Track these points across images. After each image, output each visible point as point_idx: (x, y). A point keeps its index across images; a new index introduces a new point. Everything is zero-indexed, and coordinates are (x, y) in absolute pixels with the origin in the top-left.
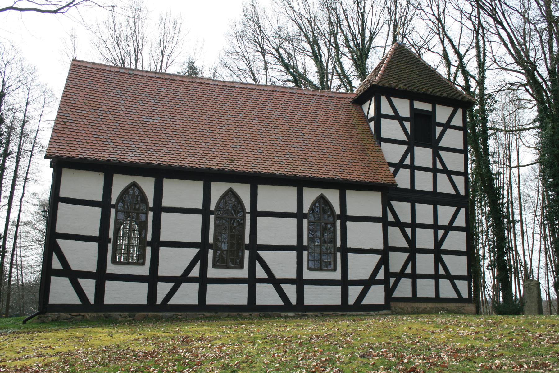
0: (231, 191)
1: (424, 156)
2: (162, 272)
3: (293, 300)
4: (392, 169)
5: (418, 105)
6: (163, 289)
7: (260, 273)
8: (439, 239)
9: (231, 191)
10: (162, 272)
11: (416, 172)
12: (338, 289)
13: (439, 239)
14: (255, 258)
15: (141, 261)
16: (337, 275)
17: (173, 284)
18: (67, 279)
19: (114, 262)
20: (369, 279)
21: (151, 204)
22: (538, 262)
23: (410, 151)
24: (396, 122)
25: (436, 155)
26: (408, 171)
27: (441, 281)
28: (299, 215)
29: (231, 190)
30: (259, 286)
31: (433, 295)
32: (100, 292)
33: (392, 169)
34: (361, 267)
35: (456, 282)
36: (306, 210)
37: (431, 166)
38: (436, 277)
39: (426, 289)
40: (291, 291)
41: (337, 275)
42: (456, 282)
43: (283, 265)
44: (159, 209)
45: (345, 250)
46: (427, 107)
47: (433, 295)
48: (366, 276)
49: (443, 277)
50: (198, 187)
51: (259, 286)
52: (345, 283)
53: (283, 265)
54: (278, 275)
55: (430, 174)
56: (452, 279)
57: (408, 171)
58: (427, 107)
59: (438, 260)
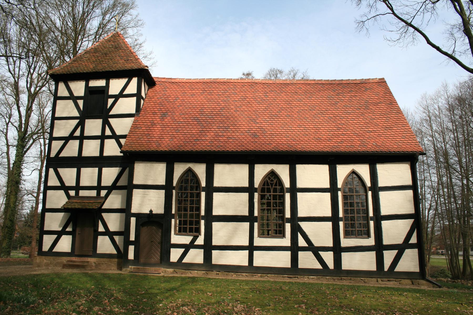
0: (190, 170)
1: (93, 126)
2: (386, 241)
3: (331, 265)
4: (123, 141)
5: (94, 83)
6: (389, 256)
7: (302, 242)
9: (190, 170)
10: (386, 241)
12: (373, 254)
14: (296, 230)
15: (280, 233)
16: (371, 242)
17: (397, 251)
18: (311, 252)
19: (259, 236)
20: (404, 242)
21: (203, 184)
23: (81, 124)
24: (121, 99)
25: (106, 123)
28: (250, 190)
29: (354, 172)
30: (300, 254)
32: (338, 261)
33: (123, 141)
34: (395, 232)
36: (256, 185)
40: (328, 257)
41: (371, 242)
43: (321, 234)
44: (294, 190)
45: (211, 218)
46: (101, 83)
48: (400, 241)
50: (243, 170)
51: (300, 254)
52: (379, 248)
53: (321, 234)
54: (316, 243)
55: (85, 141)
58: (101, 83)
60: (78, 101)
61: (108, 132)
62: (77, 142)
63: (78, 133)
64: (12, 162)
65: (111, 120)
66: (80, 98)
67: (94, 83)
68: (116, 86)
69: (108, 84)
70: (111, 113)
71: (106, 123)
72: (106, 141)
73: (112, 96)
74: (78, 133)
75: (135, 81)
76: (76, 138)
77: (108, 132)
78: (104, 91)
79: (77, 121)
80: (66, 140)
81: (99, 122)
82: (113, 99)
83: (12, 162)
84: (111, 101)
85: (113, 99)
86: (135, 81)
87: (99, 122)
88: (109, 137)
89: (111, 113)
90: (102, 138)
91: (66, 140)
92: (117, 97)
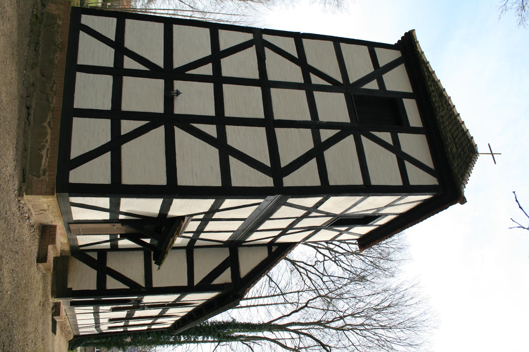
1: (334, 108)
5: (410, 107)
8: (338, 131)
11: (226, 87)
13: (338, 131)
22: (252, 308)
23: (334, 86)
25: (344, 130)
26: (386, 77)
27: (106, 123)
31: (78, 104)
35: (107, 157)
37: (262, 115)
38: (116, 114)
39: (91, 91)
42: (107, 157)
46: (414, 118)
47: (78, 104)
49: (115, 128)
55: (229, 112)
56: (114, 146)
57: (386, 77)
58: (414, 118)
59: (152, 120)
60: (375, 82)
61: (326, 134)
62: (230, 129)
63: (211, 130)
64: (276, 322)
65: (349, 140)
66: (381, 83)
67: (410, 107)
68: (415, 145)
69: (415, 131)
70: (364, 139)
71: (344, 130)
72: (308, 132)
73: (396, 140)
74: (211, 130)
75: (430, 180)
76: (222, 133)
77: (326, 134)
78: (399, 124)
79: (340, 79)
80: (226, 152)
81: (344, 117)
82: (390, 142)
83: (276, 322)
84: (386, 137)
85: (390, 142)
86: (430, 180)
87: (344, 117)
88: (316, 137)
89: (364, 139)
90: (315, 125)
91: (226, 152)
92: (395, 148)
